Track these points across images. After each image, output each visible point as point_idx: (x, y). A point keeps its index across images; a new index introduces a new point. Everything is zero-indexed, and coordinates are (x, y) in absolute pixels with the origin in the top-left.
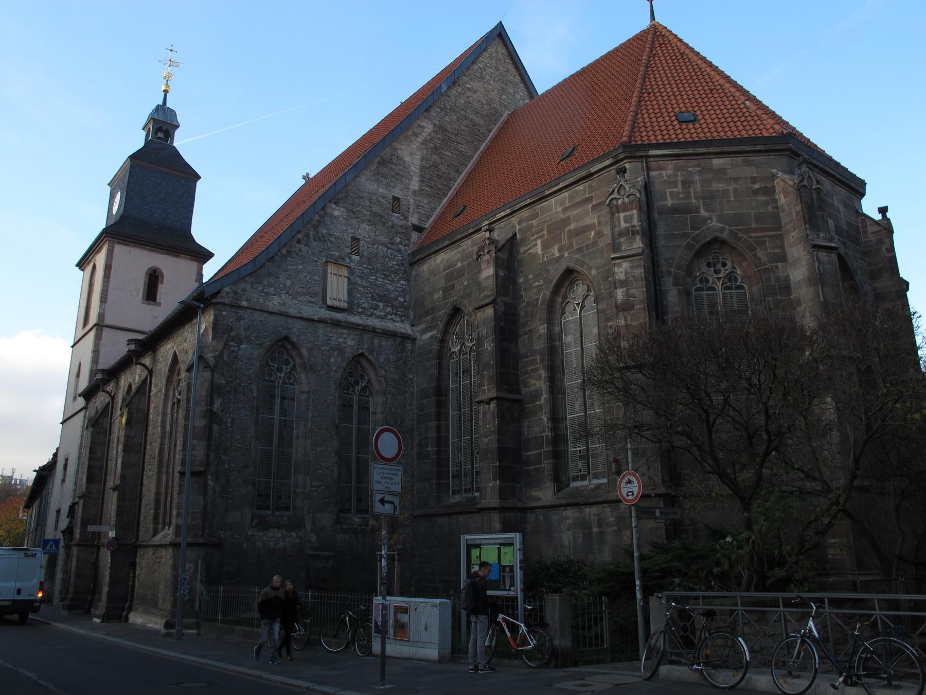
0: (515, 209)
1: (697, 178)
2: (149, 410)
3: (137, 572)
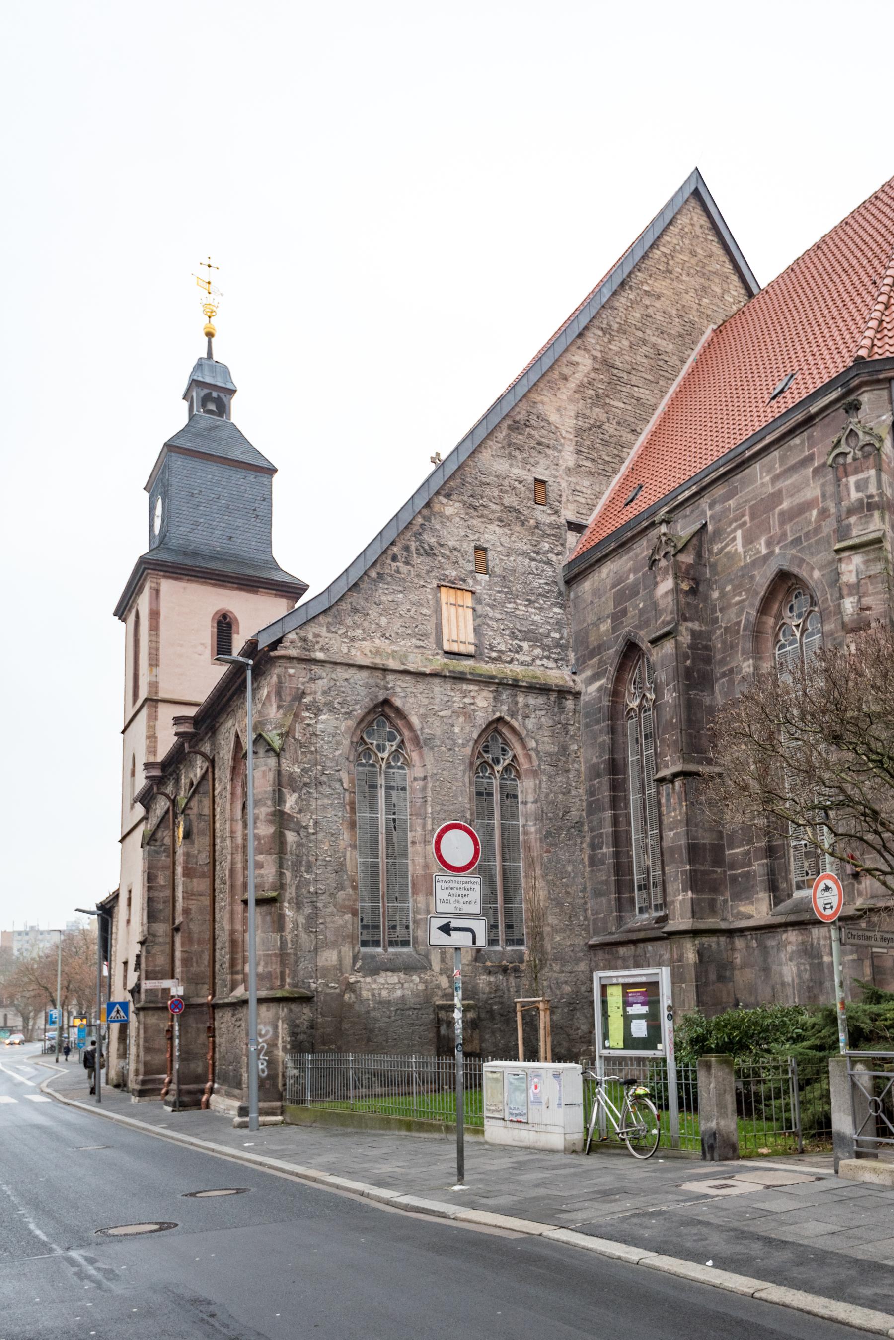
0: (704, 484)
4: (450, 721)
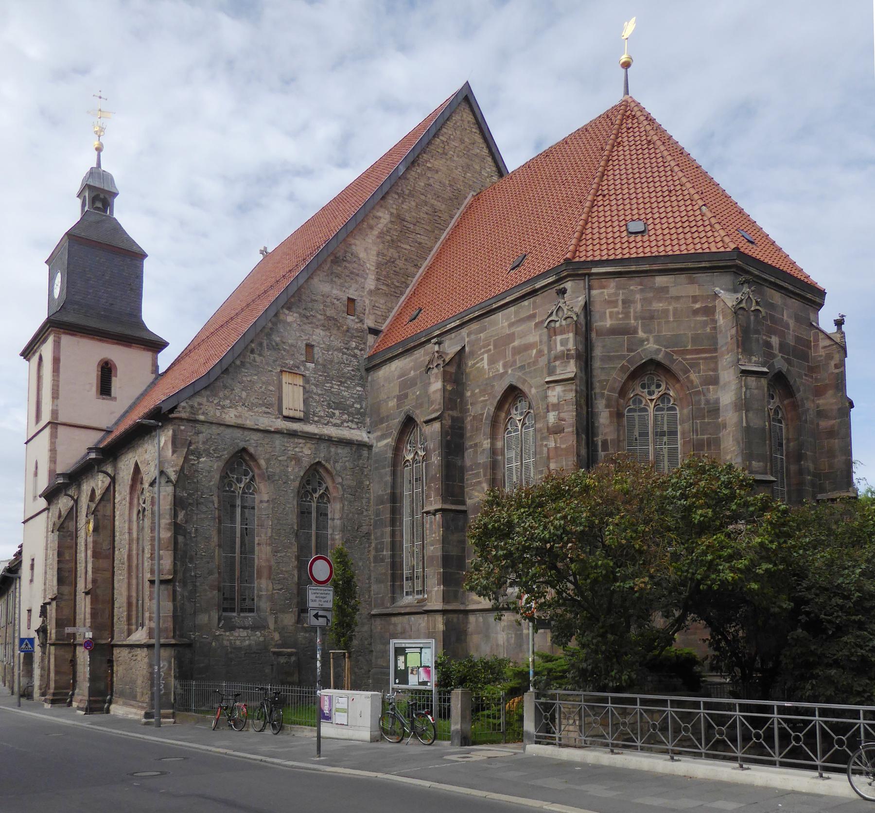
1: (638, 297)
2: (114, 517)
3: (115, 669)
4: (285, 464)
